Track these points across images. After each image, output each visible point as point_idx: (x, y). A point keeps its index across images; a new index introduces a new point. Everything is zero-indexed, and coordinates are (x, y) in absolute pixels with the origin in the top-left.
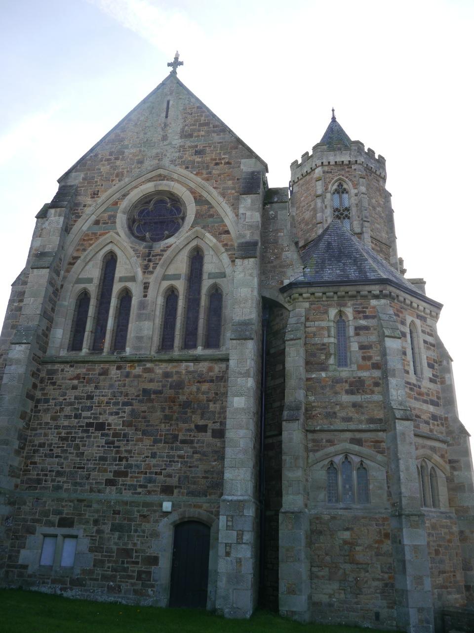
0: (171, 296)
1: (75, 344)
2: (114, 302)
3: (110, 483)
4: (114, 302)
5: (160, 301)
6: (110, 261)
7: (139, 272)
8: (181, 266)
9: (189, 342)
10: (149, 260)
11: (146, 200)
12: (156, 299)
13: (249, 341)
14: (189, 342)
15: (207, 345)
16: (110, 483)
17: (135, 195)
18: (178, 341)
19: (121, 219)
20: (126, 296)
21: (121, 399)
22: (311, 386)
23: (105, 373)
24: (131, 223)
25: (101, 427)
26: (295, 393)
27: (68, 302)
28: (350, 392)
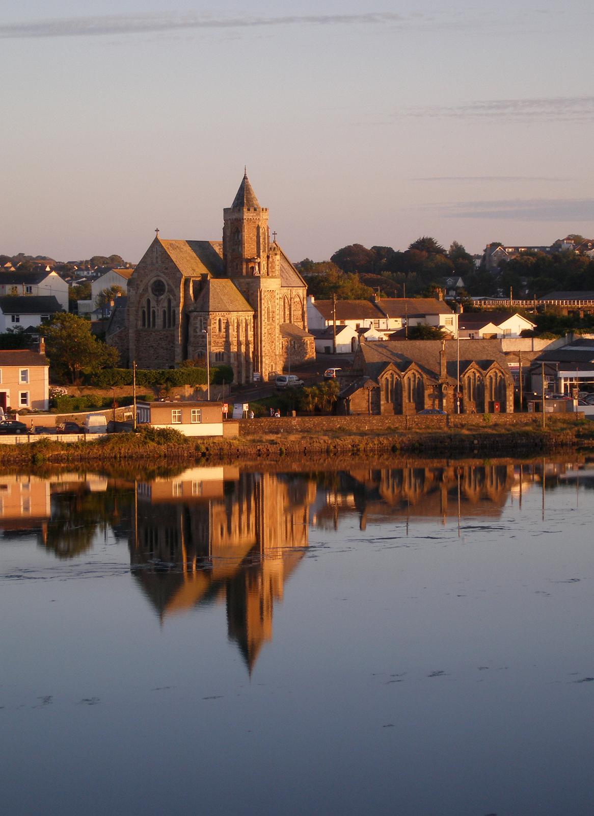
0: (164, 312)
1: (144, 325)
2: (151, 313)
3: (156, 359)
4: (151, 313)
5: (162, 313)
6: (149, 301)
7: (156, 306)
8: (166, 304)
9: (169, 326)
10: (158, 302)
11: (155, 282)
12: (161, 313)
13: (539, 350)
14: (169, 326)
15: (137, 407)
16: (156, 359)
17: (152, 281)
18: (151, 326)
19: (150, 289)
20: (154, 312)
21: (156, 340)
22: (195, 336)
23: (151, 334)
24: (152, 289)
25: (152, 346)
26: (191, 339)
27: (140, 313)
28: (202, 338)
